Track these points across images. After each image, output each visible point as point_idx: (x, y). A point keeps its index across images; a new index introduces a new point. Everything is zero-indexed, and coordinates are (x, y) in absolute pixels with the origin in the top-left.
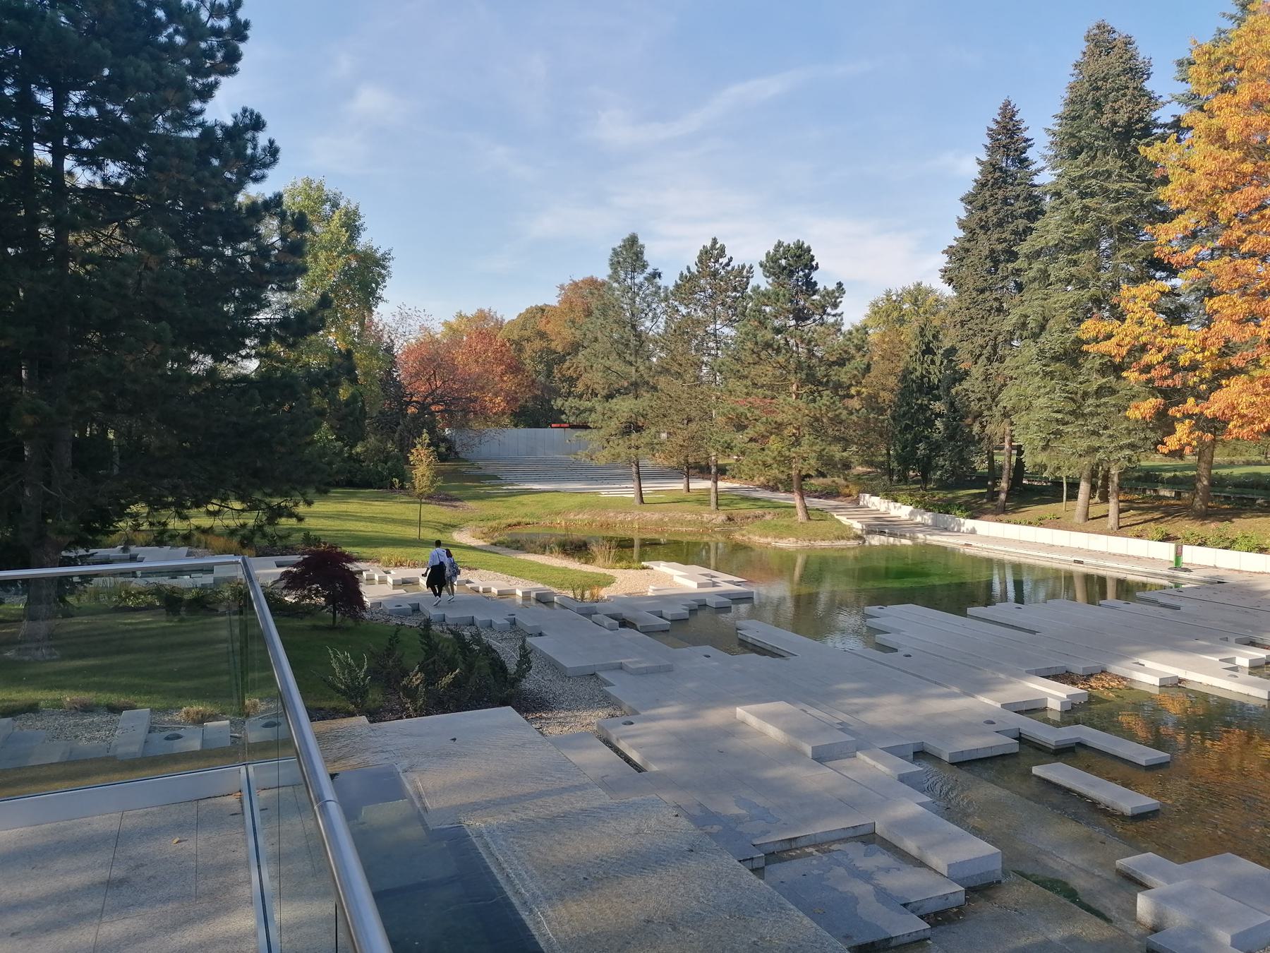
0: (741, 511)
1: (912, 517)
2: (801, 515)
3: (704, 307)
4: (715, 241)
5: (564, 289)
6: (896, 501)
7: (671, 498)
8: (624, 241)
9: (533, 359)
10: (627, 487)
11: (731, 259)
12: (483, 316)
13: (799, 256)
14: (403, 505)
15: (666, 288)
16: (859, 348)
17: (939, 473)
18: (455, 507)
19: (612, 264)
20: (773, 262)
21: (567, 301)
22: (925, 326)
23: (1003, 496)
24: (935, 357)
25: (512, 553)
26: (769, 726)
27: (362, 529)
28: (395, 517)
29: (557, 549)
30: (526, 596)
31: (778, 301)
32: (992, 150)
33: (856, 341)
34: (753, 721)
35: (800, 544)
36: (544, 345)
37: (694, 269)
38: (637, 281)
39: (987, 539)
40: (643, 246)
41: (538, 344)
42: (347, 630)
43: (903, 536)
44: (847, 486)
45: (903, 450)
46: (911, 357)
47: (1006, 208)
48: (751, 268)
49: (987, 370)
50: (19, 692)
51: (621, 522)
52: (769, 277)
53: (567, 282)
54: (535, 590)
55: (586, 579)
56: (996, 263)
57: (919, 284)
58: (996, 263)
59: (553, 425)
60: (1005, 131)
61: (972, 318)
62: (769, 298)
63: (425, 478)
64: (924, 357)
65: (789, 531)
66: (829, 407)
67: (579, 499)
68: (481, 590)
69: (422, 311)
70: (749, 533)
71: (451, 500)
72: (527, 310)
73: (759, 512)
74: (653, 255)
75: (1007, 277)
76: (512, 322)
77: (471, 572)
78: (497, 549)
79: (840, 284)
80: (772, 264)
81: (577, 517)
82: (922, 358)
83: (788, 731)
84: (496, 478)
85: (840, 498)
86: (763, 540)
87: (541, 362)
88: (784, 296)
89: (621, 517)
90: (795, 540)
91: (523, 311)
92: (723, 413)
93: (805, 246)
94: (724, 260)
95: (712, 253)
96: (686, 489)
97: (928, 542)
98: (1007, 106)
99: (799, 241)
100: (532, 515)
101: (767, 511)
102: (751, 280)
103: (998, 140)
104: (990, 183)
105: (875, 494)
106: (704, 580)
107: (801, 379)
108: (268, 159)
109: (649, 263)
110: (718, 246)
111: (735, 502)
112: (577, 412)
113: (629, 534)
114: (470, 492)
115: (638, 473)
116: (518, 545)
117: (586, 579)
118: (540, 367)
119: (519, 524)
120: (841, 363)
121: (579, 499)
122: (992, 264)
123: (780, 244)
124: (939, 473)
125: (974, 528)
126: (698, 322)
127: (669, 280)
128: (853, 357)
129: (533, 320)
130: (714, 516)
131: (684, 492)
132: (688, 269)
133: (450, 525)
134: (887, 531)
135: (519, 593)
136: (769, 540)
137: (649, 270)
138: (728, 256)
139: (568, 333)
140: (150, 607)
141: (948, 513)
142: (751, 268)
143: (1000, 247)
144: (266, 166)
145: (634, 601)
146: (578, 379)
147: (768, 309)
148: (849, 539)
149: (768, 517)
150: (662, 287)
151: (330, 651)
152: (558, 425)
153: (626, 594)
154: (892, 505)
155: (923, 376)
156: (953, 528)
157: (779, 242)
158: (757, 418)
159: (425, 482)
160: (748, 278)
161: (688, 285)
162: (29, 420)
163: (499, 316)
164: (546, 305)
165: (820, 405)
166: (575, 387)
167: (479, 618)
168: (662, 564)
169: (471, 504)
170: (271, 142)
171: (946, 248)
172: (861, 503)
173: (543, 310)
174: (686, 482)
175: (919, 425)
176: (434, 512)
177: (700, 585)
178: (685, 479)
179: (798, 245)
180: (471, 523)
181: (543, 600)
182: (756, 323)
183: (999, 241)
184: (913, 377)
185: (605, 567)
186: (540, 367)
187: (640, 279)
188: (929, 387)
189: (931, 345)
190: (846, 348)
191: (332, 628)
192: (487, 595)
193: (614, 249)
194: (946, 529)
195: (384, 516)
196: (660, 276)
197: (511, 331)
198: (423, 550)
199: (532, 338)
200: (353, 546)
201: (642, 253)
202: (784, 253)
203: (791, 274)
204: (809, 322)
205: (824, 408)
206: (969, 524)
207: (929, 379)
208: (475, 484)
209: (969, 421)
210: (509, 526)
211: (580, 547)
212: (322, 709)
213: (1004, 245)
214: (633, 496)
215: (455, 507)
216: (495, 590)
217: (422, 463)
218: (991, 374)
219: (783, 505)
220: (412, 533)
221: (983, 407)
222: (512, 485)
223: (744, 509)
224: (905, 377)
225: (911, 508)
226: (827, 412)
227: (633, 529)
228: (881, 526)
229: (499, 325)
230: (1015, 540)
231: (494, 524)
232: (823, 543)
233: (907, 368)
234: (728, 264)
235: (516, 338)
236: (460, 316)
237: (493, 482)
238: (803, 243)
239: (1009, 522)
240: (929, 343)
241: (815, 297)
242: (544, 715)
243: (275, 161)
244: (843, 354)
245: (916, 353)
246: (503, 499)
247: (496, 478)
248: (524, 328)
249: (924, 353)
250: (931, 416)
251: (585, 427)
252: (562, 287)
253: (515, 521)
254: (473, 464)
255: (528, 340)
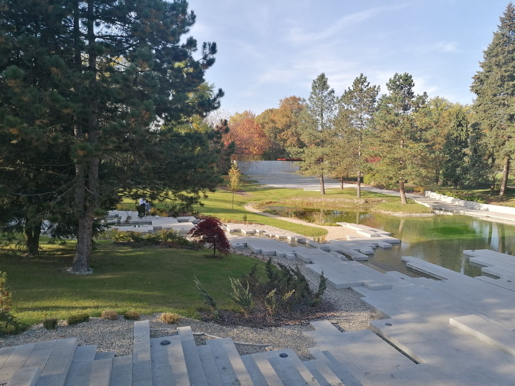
0: (371, 198)
1: (453, 202)
2: (403, 201)
3: (355, 106)
4: (362, 75)
5: (281, 101)
6: (445, 195)
7: (335, 192)
8: (319, 77)
9: (268, 131)
10: (314, 187)
11: (369, 83)
12: (247, 114)
13: (406, 80)
14: (222, 193)
15: (338, 97)
16: (436, 123)
17: (468, 182)
18: (243, 194)
19: (313, 88)
20: (393, 83)
21: (283, 106)
22: (459, 113)
23: (502, 193)
24: (463, 128)
25: (273, 216)
26: (477, 332)
27: (208, 204)
28: (220, 199)
29: (293, 215)
30: (293, 240)
31: (396, 101)
32: (501, 28)
33: (434, 119)
34: (464, 329)
35: (405, 215)
36: (274, 125)
37: (352, 88)
38: (324, 94)
39: (495, 213)
40: (327, 79)
41: (271, 125)
42: (221, 258)
43: (448, 211)
44: (417, 187)
45: (446, 171)
46: (452, 128)
47: (509, 55)
48: (379, 87)
49: (498, 133)
50: (76, 300)
51: (316, 202)
52: (391, 90)
53: (283, 99)
54: (297, 237)
55: (315, 231)
56: (503, 81)
57: (438, 97)
58: (503, 81)
59: (278, 159)
60: (510, 18)
61: (490, 109)
62: (391, 100)
63: (236, 182)
64: (458, 128)
65: (398, 208)
66: (422, 151)
67: (295, 192)
68: (271, 235)
69: (226, 111)
70: (378, 209)
71: (241, 191)
72: (265, 111)
73: (379, 199)
74: (331, 84)
75: (509, 89)
76: (259, 116)
77: (262, 226)
78: (267, 214)
79: (425, 93)
80: (393, 84)
81: (296, 200)
82: (457, 129)
83: (499, 339)
84: (256, 182)
85: (414, 193)
86: (386, 212)
87: (272, 133)
88: (400, 98)
89: (316, 200)
90: (402, 213)
91: (264, 111)
92: (368, 154)
93: (409, 75)
94: (366, 84)
95: (360, 81)
96: (341, 188)
97: (466, 215)
98: (510, 6)
99: (406, 73)
100: (276, 198)
101: (383, 198)
102: (379, 93)
103: (505, 23)
104: (502, 43)
105: (432, 191)
106: (373, 233)
107: (408, 137)
108: (191, 21)
109: (330, 86)
110: (363, 77)
111: (366, 194)
112: (297, 153)
113: (319, 207)
114: (248, 188)
115: (323, 181)
116: (275, 213)
117: (315, 231)
118: (272, 135)
119: (271, 202)
120: (426, 130)
121: (295, 192)
122: (501, 83)
123: (396, 75)
124: (468, 182)
125: (488, 208)
126: (353, 113)
127: (339, 93)
128: (433, 127)
129: (268, 115)
130: (359, 201)
131: (341, 189)
132: (349, 88)
133: (242, 203)
134: (443, 209)
135: (289, 238)
136: (389, 212)
137: (330, 89)
138: (368, 82)
139: (285, 120)
140: (128, 244)
141: (472, 201)
142: (379, 87)
143: (506, 74)
144: (190, 24)
145: (342, 243)
146: (287, 140)
147: (390, 105)
148: (429, 213)
149: (384, 201)
150: (336, 97)
151: (231, 279)
152: (281, 159)
153: (337, 239)
154: (442, 196)
155: (457, 137)
156: (477, 208)
157: (396, 74)
158: (385, 156)
159: (236, 184)
160: (377, 91)
161: (348, 95)
162: (81, 153)
163: (253, 114)
164: (273, 109)
165: (418, 149)
166: (286, 143)
167: (279, 252)
168: (348, 224)
169: (249, 193)
170: (192, 12)
171: (473, 76)
172: (426, 195)
173: (272, 111)
174: (342, 185)
175: (455, 160)
176: (238, 197)
177: (372, 236)
178: (341, 183)
179: (406, 74)
180: (251, 202)
181: (301, 242)
182: (385, 112)
183: (506, 71)
184: (453, 137)
185: (319, 225)
186: (272, 135)
187: (325, 93)
188: (460, 142)
189: (461, 122)
190: (430, 123)
191: (214, 257)
192: (274, 238)
193: (314, 81)
194: (472, 208)
195: (214, 198)
196: (334, 92)
197: (259, 120)
198: (237, 215)
199: (269, 123)
200: (207, 212)
201: (326, 82)
202: (398, 79)
203: (402, 88)
204: (409, 111)
205: (419, 151)
206: (485, 206)
207: (460, 138)
208: (249, 184)
209: (486, 157)
210: (267, 203)
211: (302, 214)
212: (227, 310)
213: (508, 73)
214: (320, 191)
215: (243, 194)
216: (277, 236)
217: (234, 177)
218: (500, 135)
219: (389, 196)
220: (229, 206)
221: (495, 151)
222: (264, 185)
223: (372, 198)
224: (448, 137)
225: (453, 198)
226: (421, 153)
227: (322, 206)
228: (440, 207)
229: (253, 116)
230: (511, 215)
231: (261, 202)
232: (416, 215)
233: (450, 133)
234: (368, 86)
235: (262, 122)
236: (237, 114)
237: (256, 184)
238: (408, 74)
239: (506, 206)
240: (460, 121)
241: (413, 99)
242: (335, 314)
243: (194, 22)
244: (428, 125)
245: (454, 126)
246: (262, 191)
247: (256, 182)
248: (264, 118)
249: (458, 126)
250: (461, 155)
251: (300, 160)
252: (281, 101)
253: (269, 201)
254: (246, 176)
255: (267, 123)
